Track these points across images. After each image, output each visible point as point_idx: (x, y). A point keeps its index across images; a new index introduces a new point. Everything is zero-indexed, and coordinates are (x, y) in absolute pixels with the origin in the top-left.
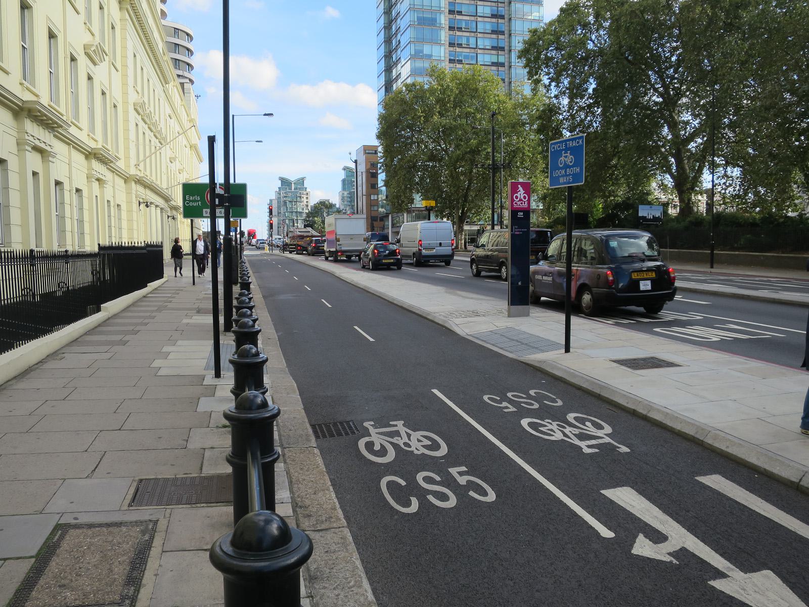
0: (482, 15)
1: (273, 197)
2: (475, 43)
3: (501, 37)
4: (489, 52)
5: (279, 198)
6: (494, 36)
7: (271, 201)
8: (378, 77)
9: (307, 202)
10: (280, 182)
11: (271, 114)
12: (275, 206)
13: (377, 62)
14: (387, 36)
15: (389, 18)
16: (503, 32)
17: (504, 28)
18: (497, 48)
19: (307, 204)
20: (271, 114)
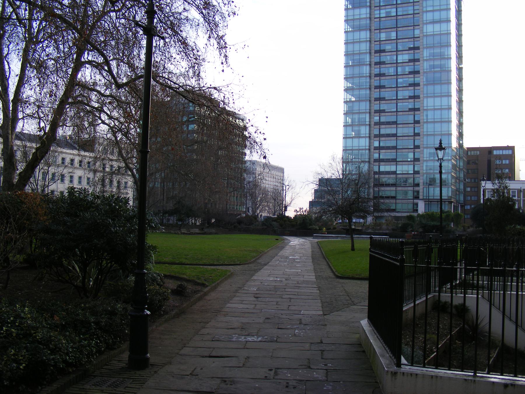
2: (395, 35)
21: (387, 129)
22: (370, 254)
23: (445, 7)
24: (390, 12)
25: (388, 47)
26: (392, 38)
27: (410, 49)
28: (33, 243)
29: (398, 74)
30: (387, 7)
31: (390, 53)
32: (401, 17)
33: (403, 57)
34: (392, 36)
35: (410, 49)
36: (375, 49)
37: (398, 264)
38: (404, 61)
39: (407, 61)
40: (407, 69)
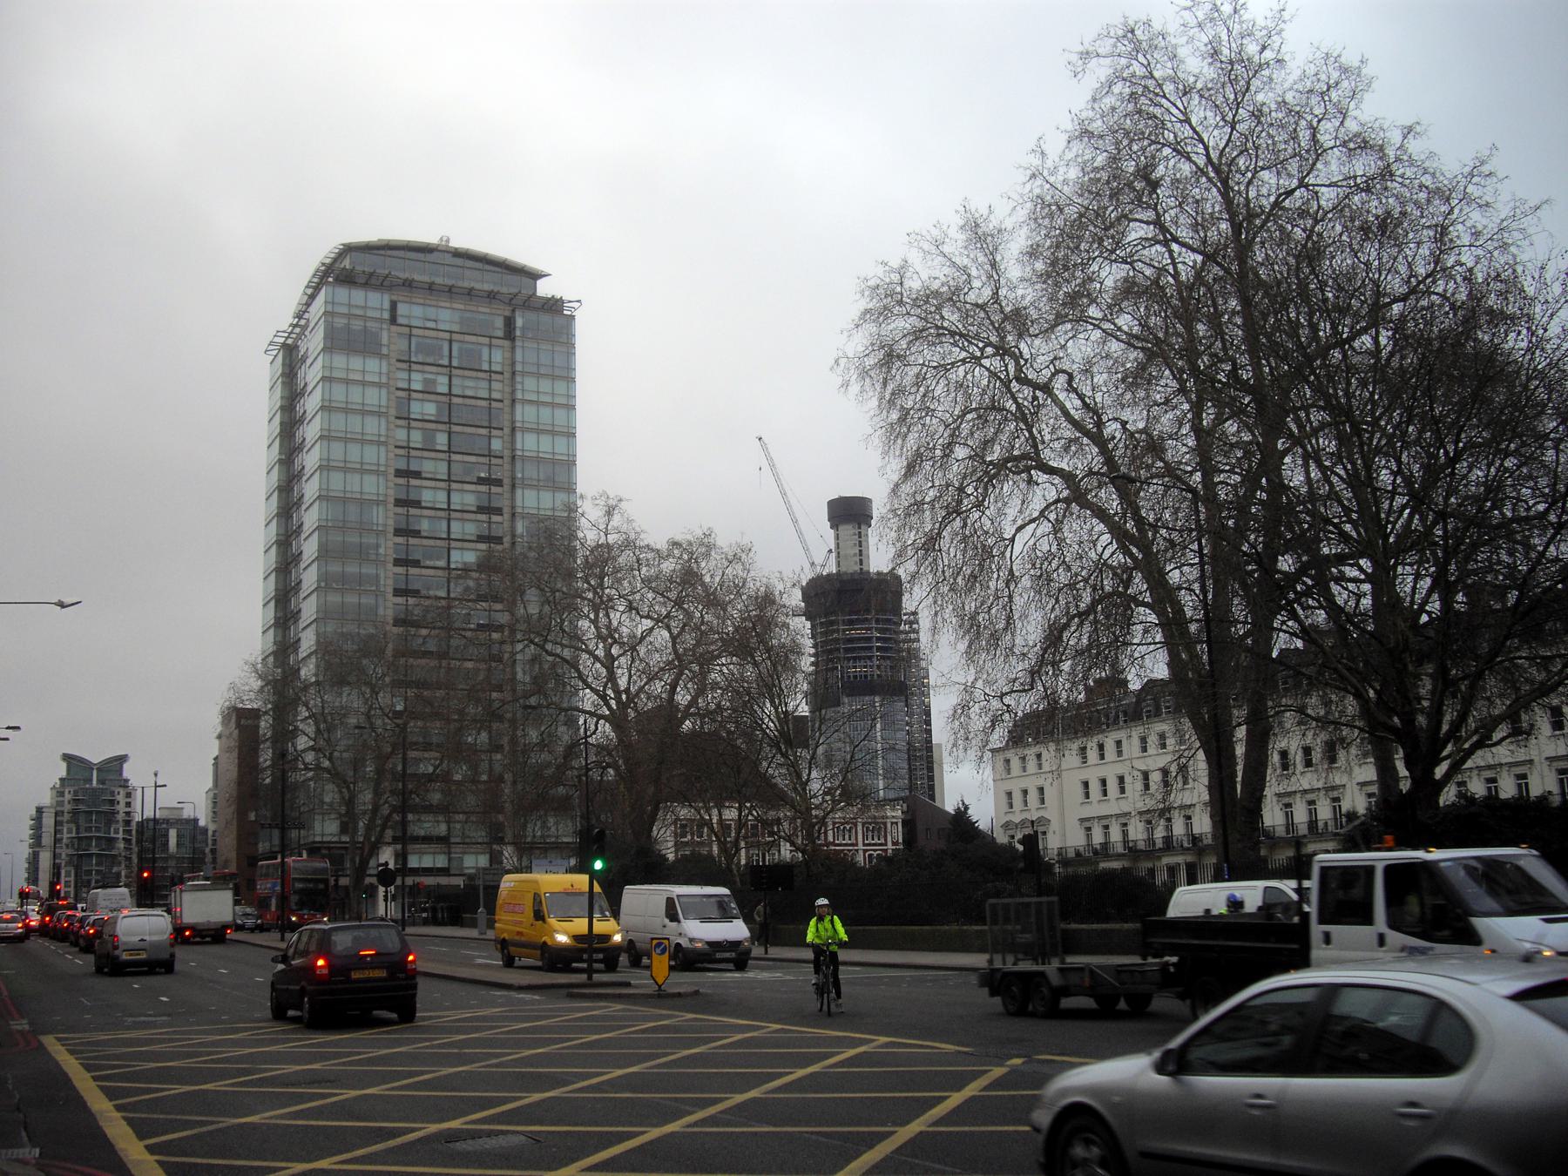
0: (458, 508)
1: (46, 799)
2: (446, 442)
3: (495, 518)
4: (472, 516)
5: (60, 803)
6: (484, 517)
7: (40, 810)
8: (266, 552)
9: (128, 814)
10: (64, 765)
11: (18, 728)
12: (48, 821)
13: (267, 419)
14: (282, 531)
15: (288, 471)
16: (501, 538)
17: (504, 503)
18: (487, 509)
19: (128, 810)
20: (18, 728)
21: (465, 553)
22: (147, 1147)
23: (563, 401)
24: (434, 382)
25: (428, 467)
26: (438, 448)
27: (481, 481)
28: (998, 964)
29: (452, 536)
30: (428, 368)
31: (432, 484)
32: (459, 401)
33: (466, 498)
34: (438, 441)
35: (481, 481)
36: (269, 1014)
37: (1295, 946)
38: (466, 508)
39: (474, 509)
40: (471, 529)
